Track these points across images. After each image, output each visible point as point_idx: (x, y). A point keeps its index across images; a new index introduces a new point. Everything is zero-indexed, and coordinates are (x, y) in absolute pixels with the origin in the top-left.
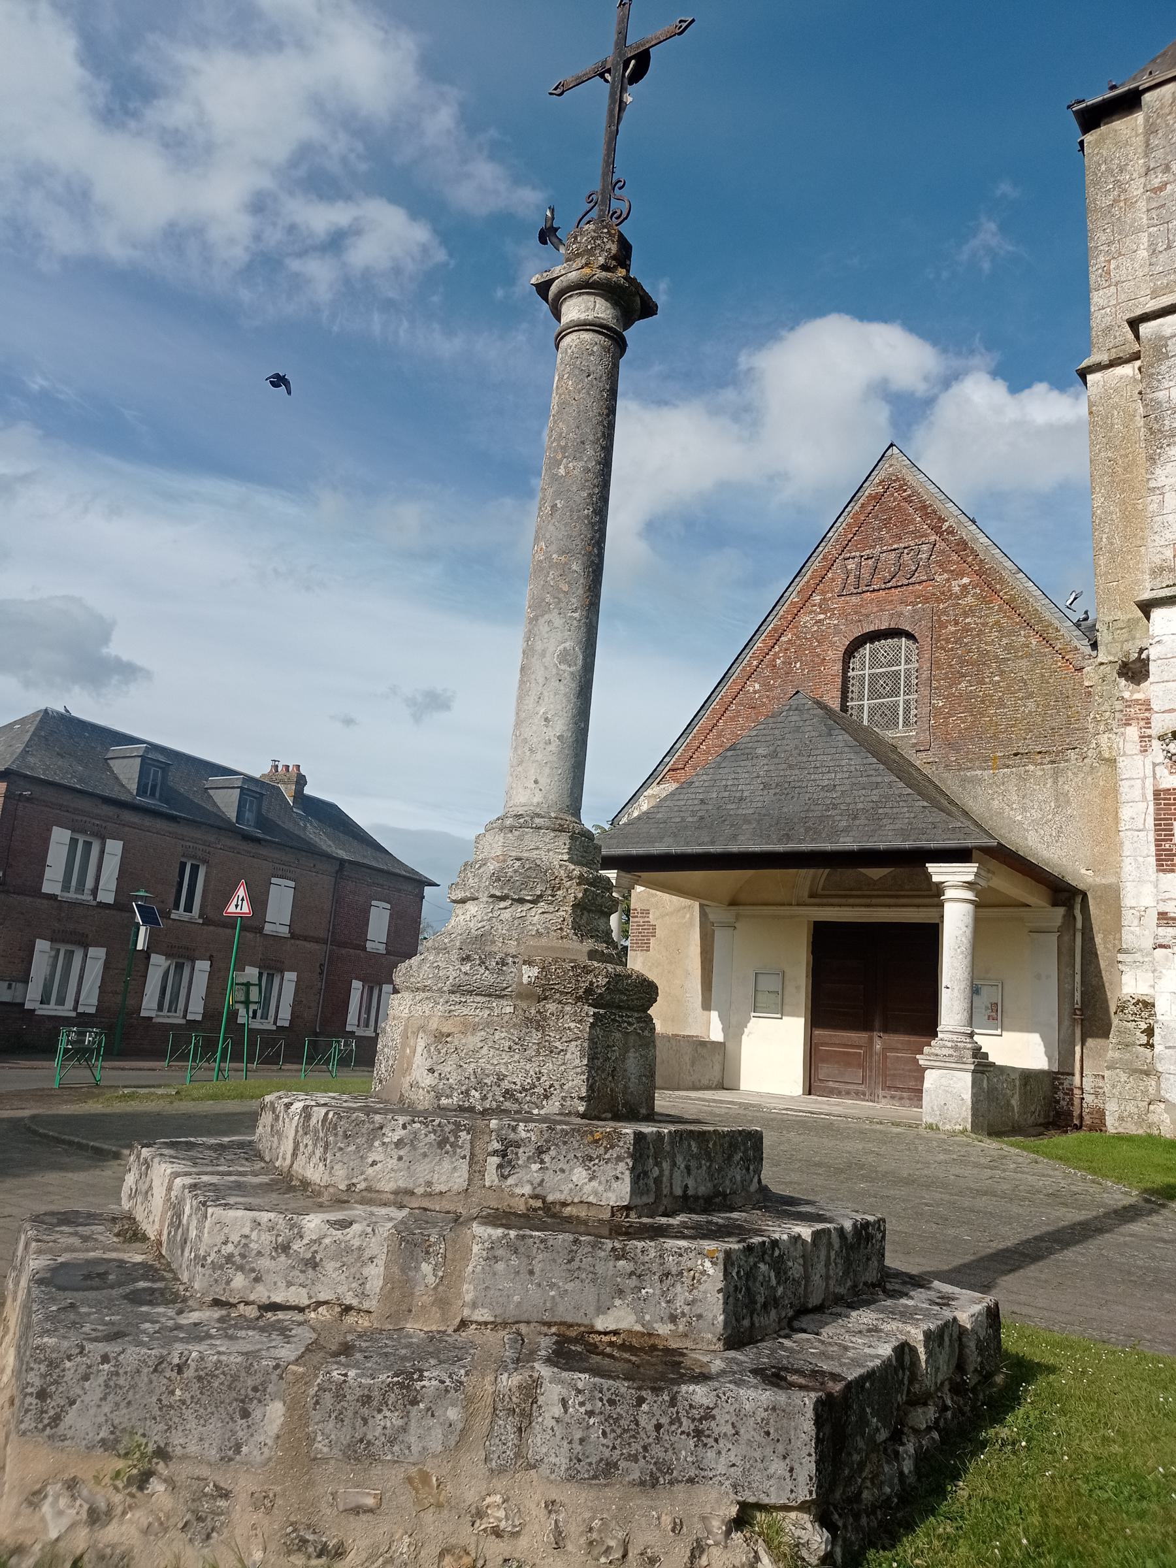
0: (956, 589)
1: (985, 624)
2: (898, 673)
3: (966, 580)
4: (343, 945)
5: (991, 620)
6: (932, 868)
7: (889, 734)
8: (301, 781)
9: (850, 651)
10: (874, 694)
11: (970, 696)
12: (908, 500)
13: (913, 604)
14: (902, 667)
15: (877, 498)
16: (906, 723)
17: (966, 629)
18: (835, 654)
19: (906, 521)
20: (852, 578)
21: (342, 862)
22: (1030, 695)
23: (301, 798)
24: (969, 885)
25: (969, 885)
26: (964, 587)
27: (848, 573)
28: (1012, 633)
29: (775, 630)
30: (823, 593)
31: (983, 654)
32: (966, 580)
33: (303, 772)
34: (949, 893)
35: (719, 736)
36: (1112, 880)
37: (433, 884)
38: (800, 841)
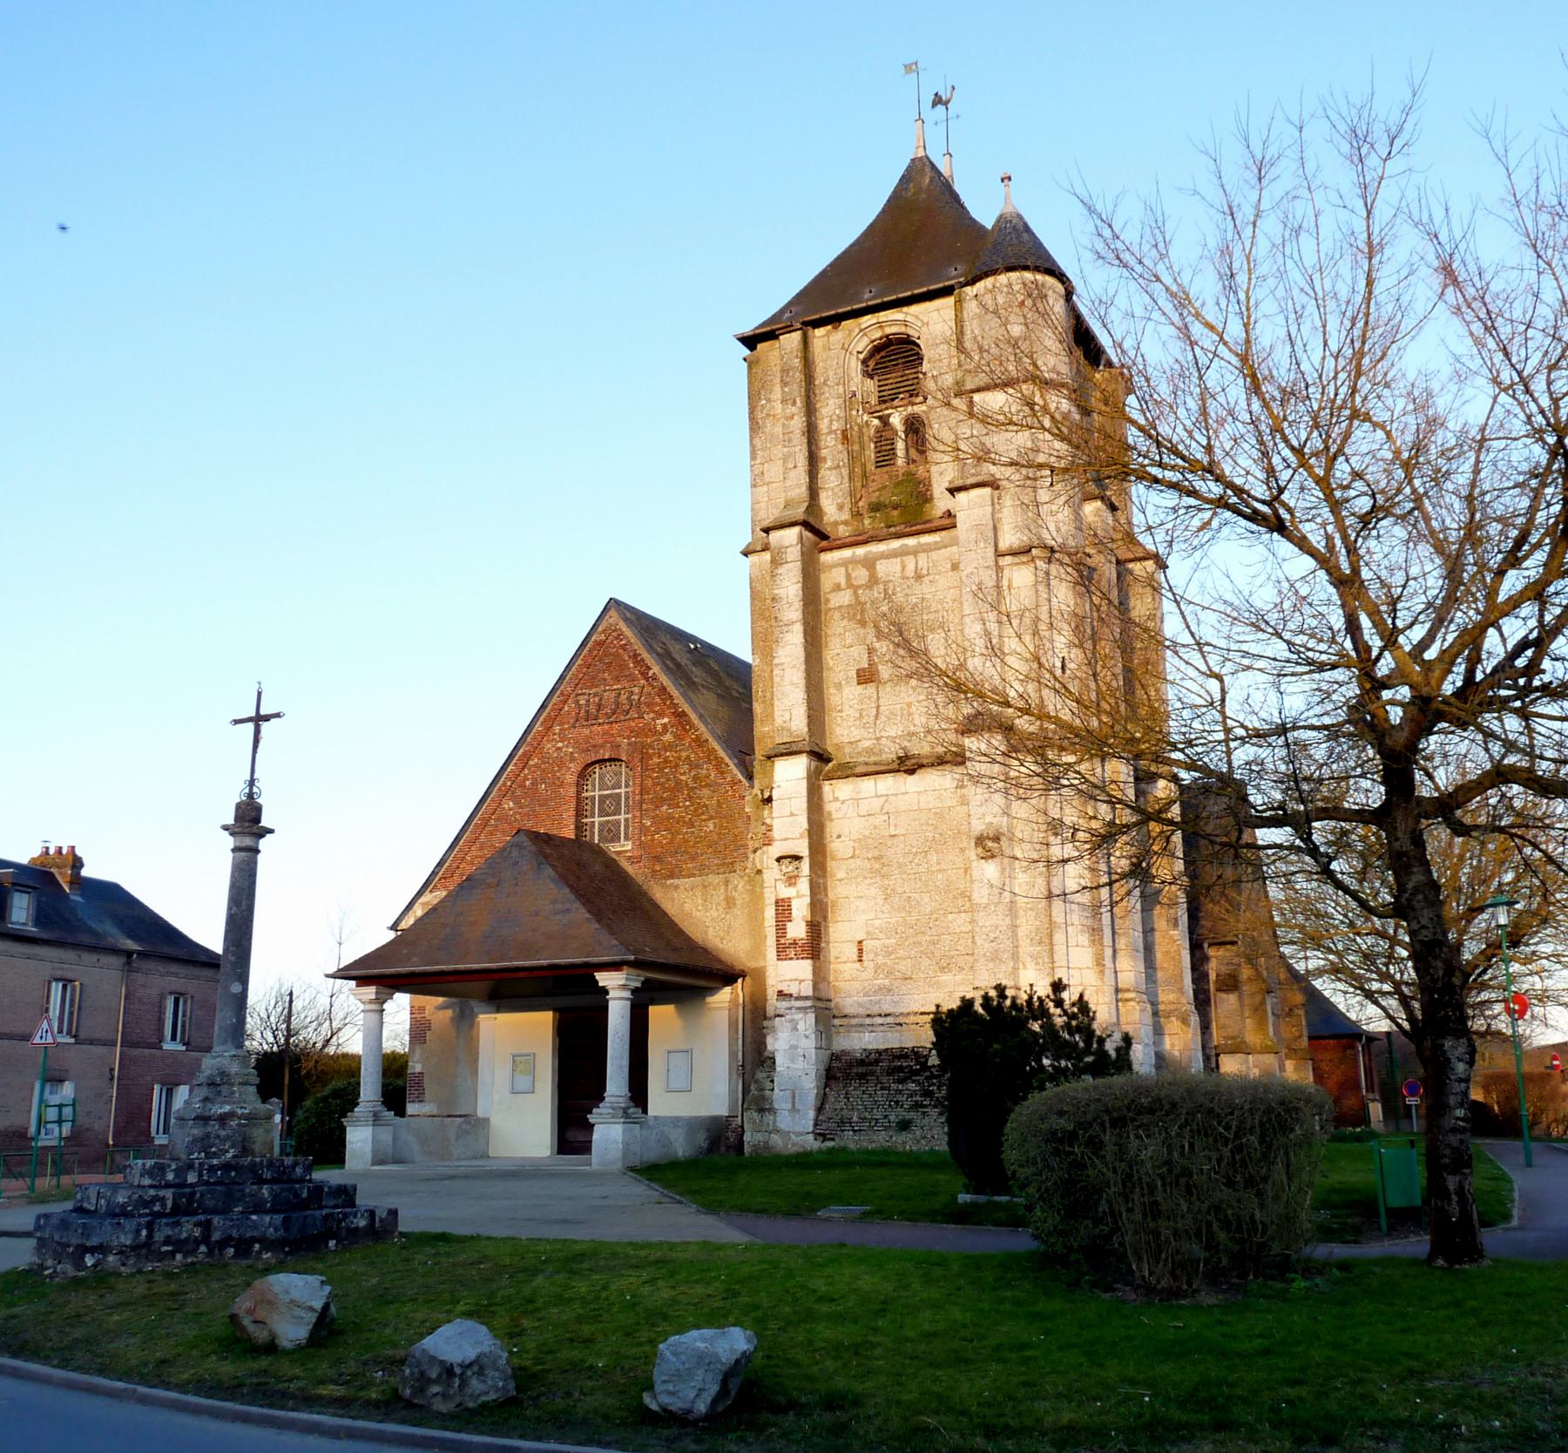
0: (659, 728)
1: (679, 758)
2: (619, 795)
3: (666, 720)
4: (136, 1045)
5: (684, 754)
6: (598, 976)
7: (613, 848)
8: (77, 863)
9: (583, 775)
10: (603, 813)
11: (670, 817)
12: (623, 647)
13: (628, 737)
14: (623, 790)
15: (600, 644)
16: (626, 838)
17: (666, 761)
18: (571, 778)
19: (623, 667)
20: (583, 713)
21: (129, 954)
22: (711, 818)
23: (80, 882)
24: (624, 987)
25: (624, 987)
26: (664, 726)
27: (580, 706)
28: (698, 766)
29: (524, 754)
30: (561, 724)
31: (678, 782)
32: (666, 720)
33: (79, 853)
34: (612, 994)
35: (481, 848)
36: (761, 964)
37: (225, 828)
38: (511, 959)
